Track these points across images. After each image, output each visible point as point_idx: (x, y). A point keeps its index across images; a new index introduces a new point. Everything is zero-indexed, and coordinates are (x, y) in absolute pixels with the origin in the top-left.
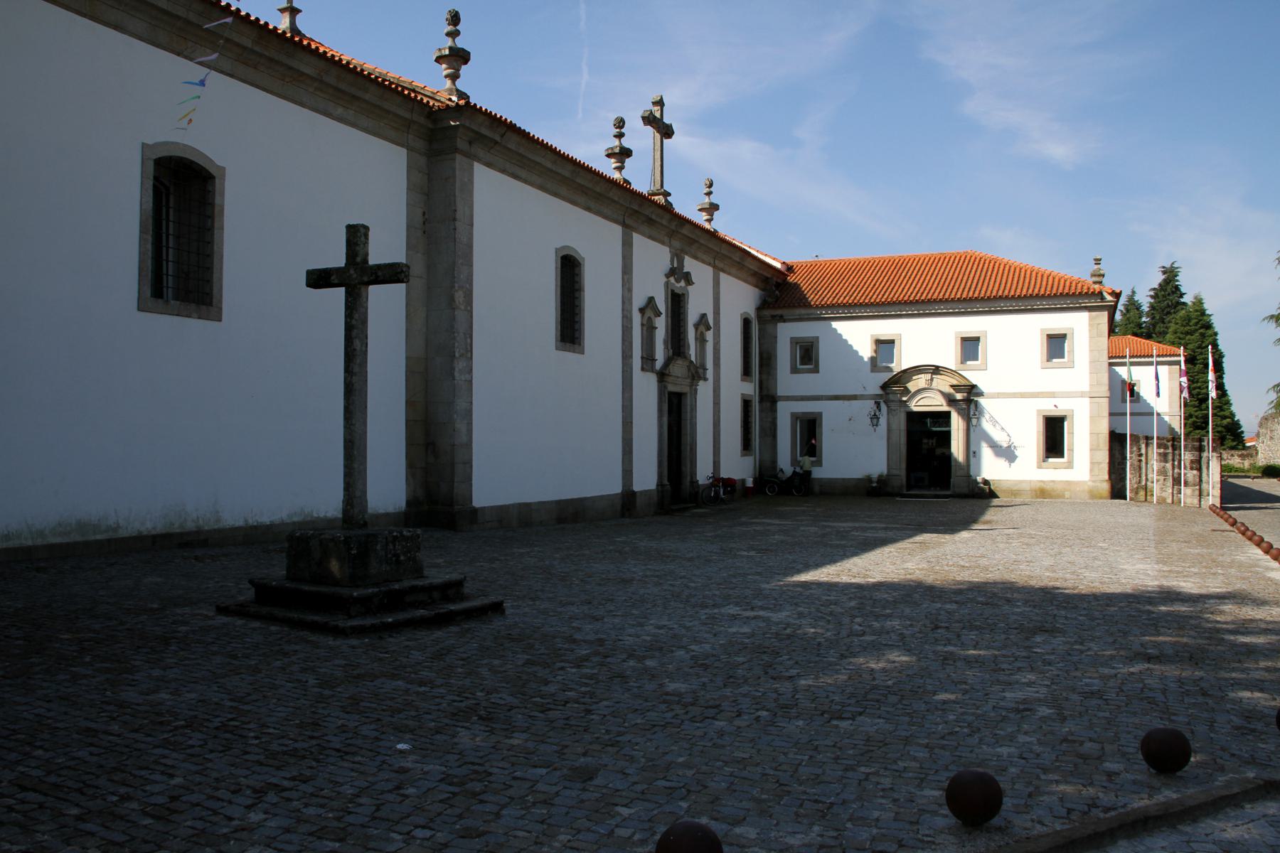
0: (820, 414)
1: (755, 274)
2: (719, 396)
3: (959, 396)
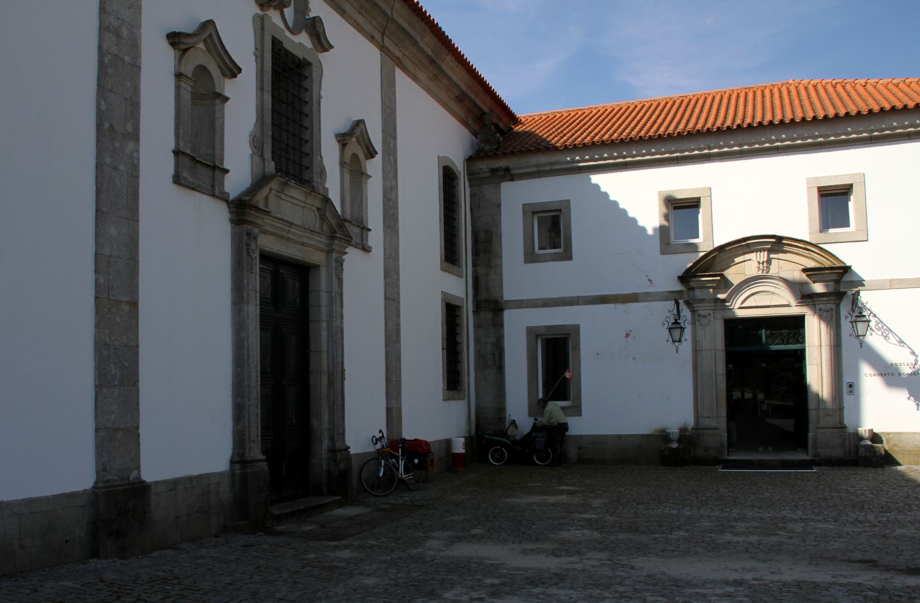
0: (576, 328)
1: (462, 98)
2: (397, 285)
3: (819, 288)
